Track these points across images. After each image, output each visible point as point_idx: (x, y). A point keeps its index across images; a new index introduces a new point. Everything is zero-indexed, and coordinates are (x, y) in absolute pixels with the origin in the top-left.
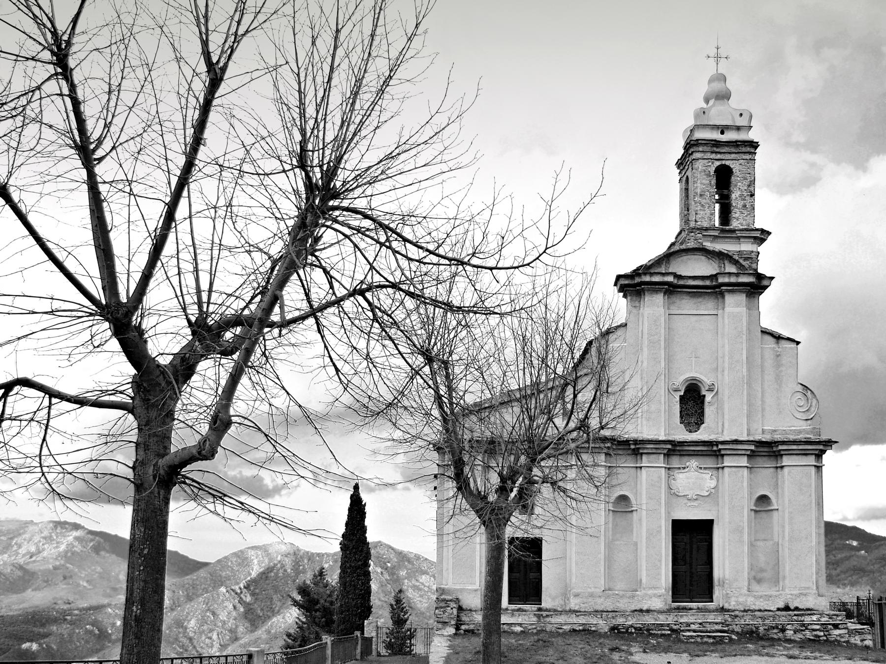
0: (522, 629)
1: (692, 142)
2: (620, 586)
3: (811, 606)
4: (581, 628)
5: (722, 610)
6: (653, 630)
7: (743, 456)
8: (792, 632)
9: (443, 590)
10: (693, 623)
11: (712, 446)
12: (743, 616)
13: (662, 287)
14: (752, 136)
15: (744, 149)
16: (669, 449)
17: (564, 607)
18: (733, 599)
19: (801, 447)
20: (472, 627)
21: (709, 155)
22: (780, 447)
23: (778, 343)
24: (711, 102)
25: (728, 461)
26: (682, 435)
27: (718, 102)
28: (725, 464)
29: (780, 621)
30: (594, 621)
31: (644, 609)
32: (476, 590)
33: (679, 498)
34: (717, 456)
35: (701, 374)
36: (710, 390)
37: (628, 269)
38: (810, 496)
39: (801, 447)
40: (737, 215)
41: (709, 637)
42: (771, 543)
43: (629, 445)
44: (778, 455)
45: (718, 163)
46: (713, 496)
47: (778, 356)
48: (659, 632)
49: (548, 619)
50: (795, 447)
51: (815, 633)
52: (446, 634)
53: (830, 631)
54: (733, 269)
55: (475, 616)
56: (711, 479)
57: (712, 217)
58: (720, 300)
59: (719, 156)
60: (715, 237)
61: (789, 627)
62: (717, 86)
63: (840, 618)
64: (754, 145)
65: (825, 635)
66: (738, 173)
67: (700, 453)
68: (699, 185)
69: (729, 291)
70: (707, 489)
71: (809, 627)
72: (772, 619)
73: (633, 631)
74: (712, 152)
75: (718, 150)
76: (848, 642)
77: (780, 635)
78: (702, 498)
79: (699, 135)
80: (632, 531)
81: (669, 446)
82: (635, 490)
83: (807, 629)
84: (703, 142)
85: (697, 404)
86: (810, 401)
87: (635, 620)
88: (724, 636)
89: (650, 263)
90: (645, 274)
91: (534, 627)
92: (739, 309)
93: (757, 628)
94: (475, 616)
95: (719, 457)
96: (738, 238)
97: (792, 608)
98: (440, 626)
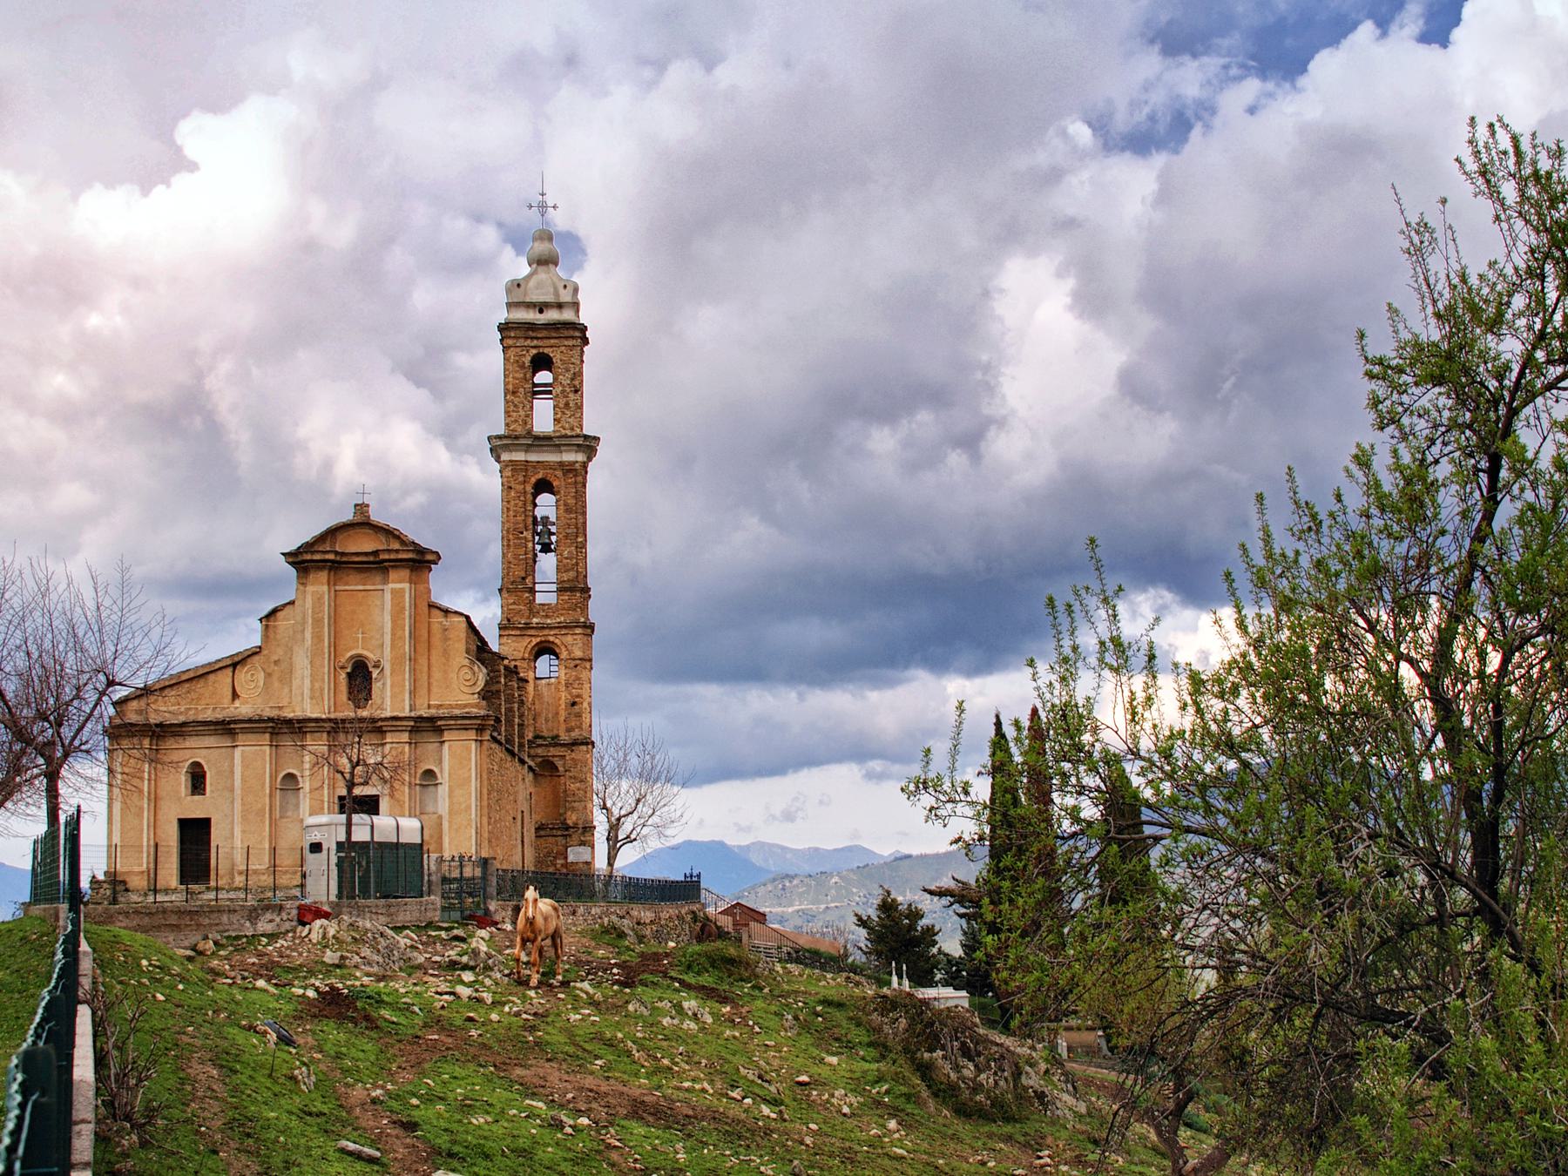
15: (566, 333)
16: (412, 727)
19: (459, 722)
22: (439, 723)
23: (446, 617)
26: (348, 713)
27: (541, 269)
28: (388, 740)
31: (433, 888)
32: (143, 872)
36: (376, 666)
37: (292, 547)
39: (459, 722)
44: (439, 731)
45: (534, 351)
50: (453, 722)
54: (396, 546)
57: (528, 419)
59: (535, 342)
69: (393, 567)
74: (526, 338)
75: (534, 335)
80: (204, 789)
90: (306, 552)
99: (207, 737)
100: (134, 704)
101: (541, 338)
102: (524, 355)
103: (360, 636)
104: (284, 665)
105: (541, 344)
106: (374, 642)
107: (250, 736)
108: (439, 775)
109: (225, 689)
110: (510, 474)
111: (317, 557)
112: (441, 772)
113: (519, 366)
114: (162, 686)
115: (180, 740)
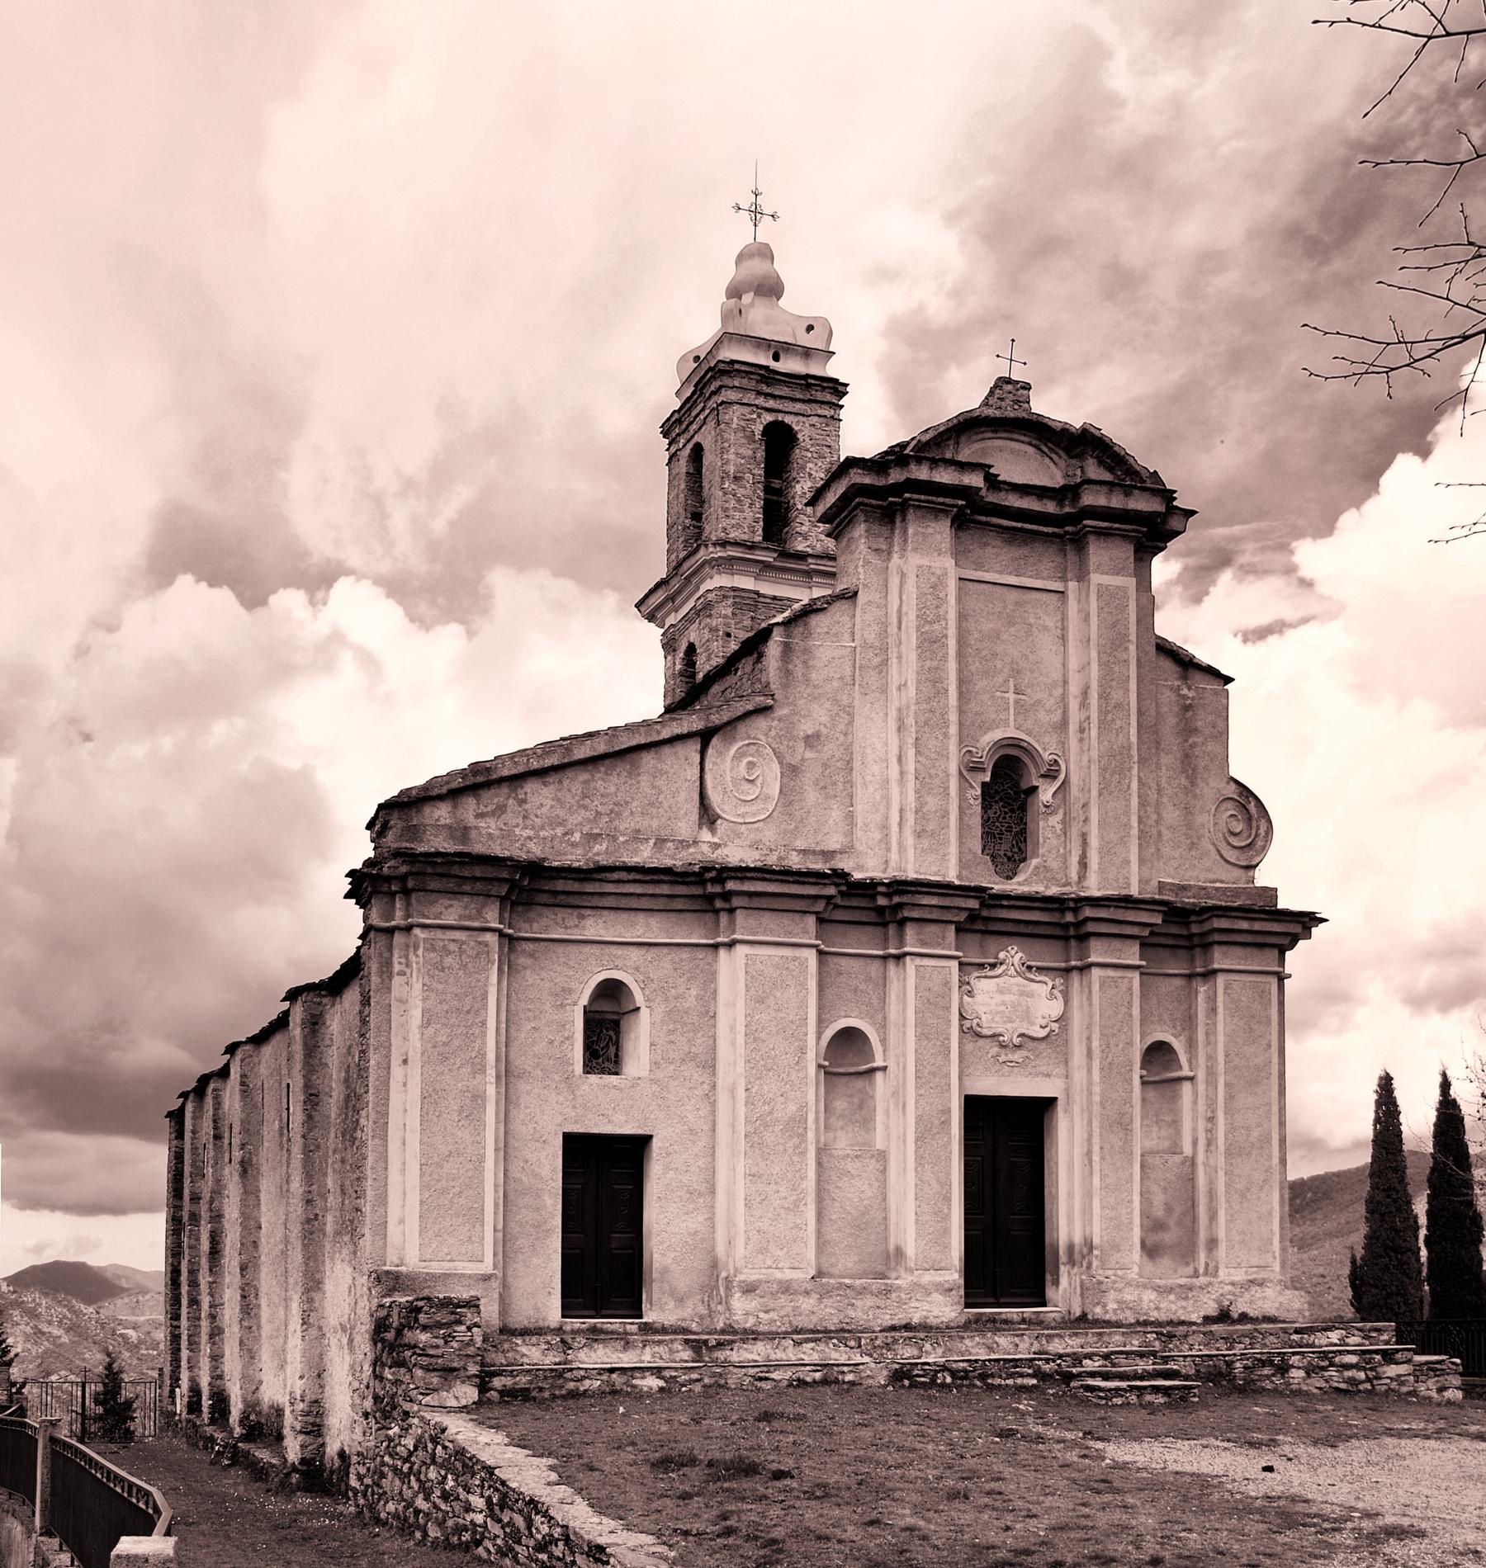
0: (661, 1383)
1: (721, 366)
2: (845, 1262)
3: (1273, 1312)
4: (818, 1375)
5: (1083, 1321)
6: (992, 1376)
7: (1129, 942)
8: (1302, 1373)
9: (397, 1276)
10: (1089, 1356)
11: (1062, 911)
12: (1186, 1336)
13: (948, 501)
14: (832, 370)
17: (707, 1322)
18: (1112, 1295)
19: (1258, 926)
20: (523, 1381)
21: (750, 398)
24: (747, 298)
25: (1098, 952)
29: (1265, 1345)
30: (838, 1355)
31: (916, 1320)
33: (981, 1042)
34: (1066, 939)
35: (1029, 734)
38: (1269, 1046)
39: (1258, 926)
40: (804, 529)
41: (1156, 1390)
42: (1177, 1159)
43: (873, 897)
44: (1205, 945)
45: (769, 418)
46: (1055, 1039)
47: (1187, 708)
48: (1010, 1382)
49: (721, 1355)
51: (1348, 1374)
52: (454, 1403)
53: (1380, 1369)
55: (524, 1350)
56: (1052, 997)
58: (1072, 556)
59: (771, 404)
60: (766, 566)
61: (1295, 1360)
62: (757, 267)
63: (1385, 1337)
64: (838, 389)
65: (1368, 1380)
66: (808, 443)
67: (1022, 929)
68: (732, 457)
70: (1044, 1022)
71: (1337, 1360)
72: (1247, 1341)
73: (949, 1380)
74: (759, 393)
76: (1413, 1393)
77: (1278, 1380)
78: (1031, 1044)
79: (729, 353)
81: (973, 904)
82: (880, 1017)
83: (1332, 1364)
84: (743, 368)
85: (1012, 811)
86: (1254, 824)
87: (940, 1351)
88: (1190, 1388)
89: (928, 437)
90: (919, 460)
91: (695, 1376)
92: (1119, 578)
93: (1229, 1364)
94: (524, 1350)
95: (1073, 943)
96: (809, 574)
97: (1235, 1316)
98: (435, 1380)
99: (641, 917)
100: (441, 813)
101: (781, 397)
102: (754, 420)
103: (1011, 696)
104: (829, 750)
105: (780, 407)
106: (1042, 716)
107: (767, 919)
108: (1183, 1058)
109: (683, 796)
110: (729, 611)
111: (945, 476)
112: (1191, 1044)
113: (745, 437)
114: (521, 769)
115: (571, 917)
